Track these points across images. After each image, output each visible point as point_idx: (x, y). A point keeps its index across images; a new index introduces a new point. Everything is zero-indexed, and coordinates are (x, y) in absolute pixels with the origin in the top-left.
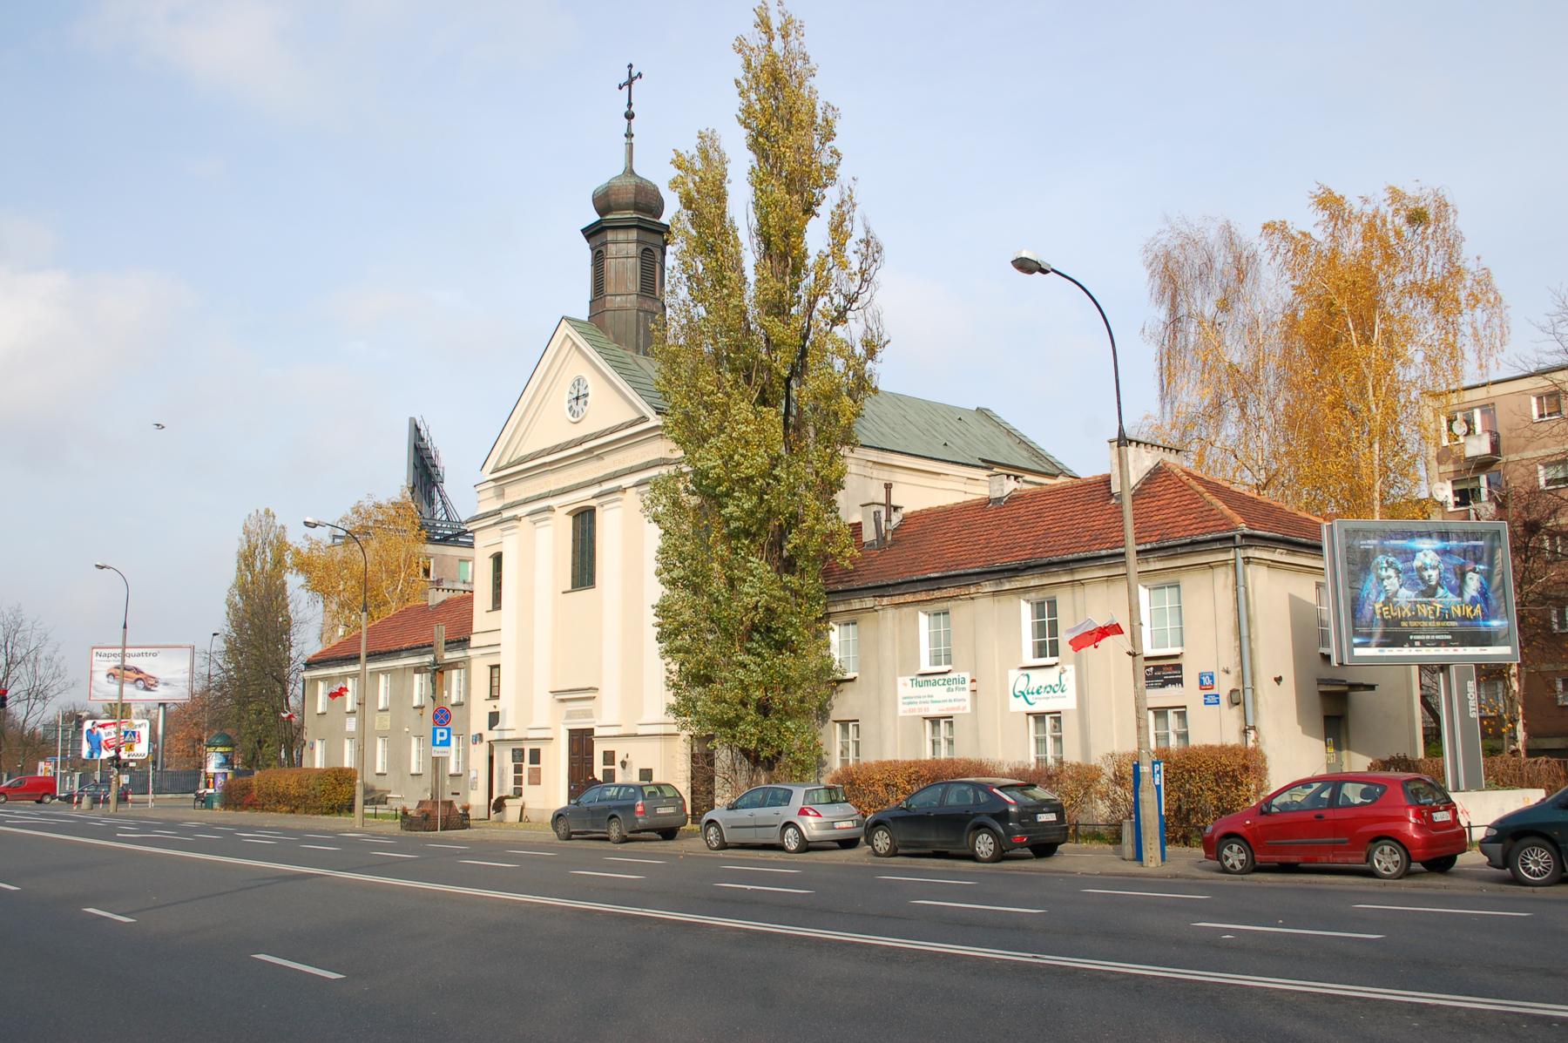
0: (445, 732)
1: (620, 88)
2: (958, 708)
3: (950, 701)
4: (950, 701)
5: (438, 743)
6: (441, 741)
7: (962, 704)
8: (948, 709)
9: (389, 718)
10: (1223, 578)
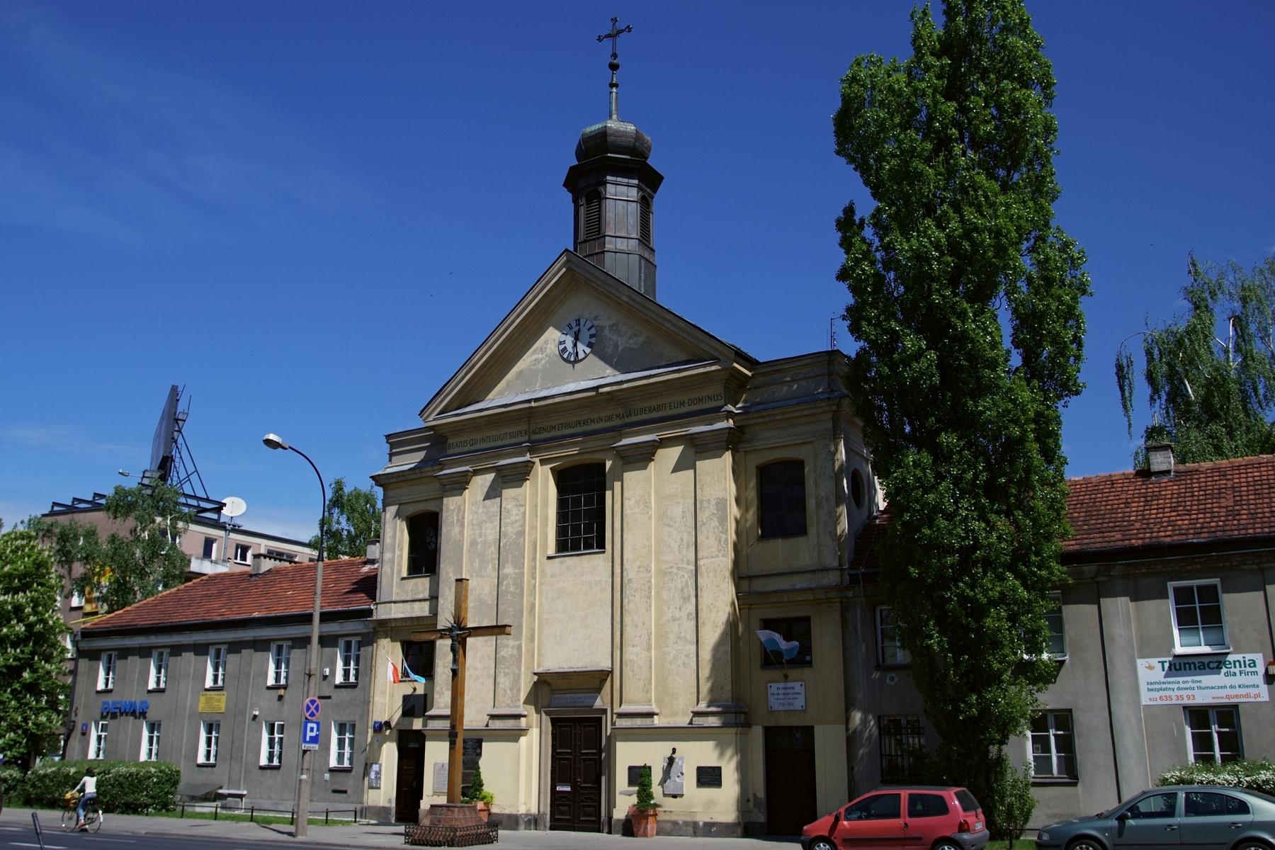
0: (315, 726)
1: (600, 39)
2: (1248, 695)
3: (1231, 687)
4: (1231, 687)
5: (308, 739)
6: (310, 737)
7: (1253, 691)
8: (1228, 697)
9: (224, 699)
10: (494, 637)
